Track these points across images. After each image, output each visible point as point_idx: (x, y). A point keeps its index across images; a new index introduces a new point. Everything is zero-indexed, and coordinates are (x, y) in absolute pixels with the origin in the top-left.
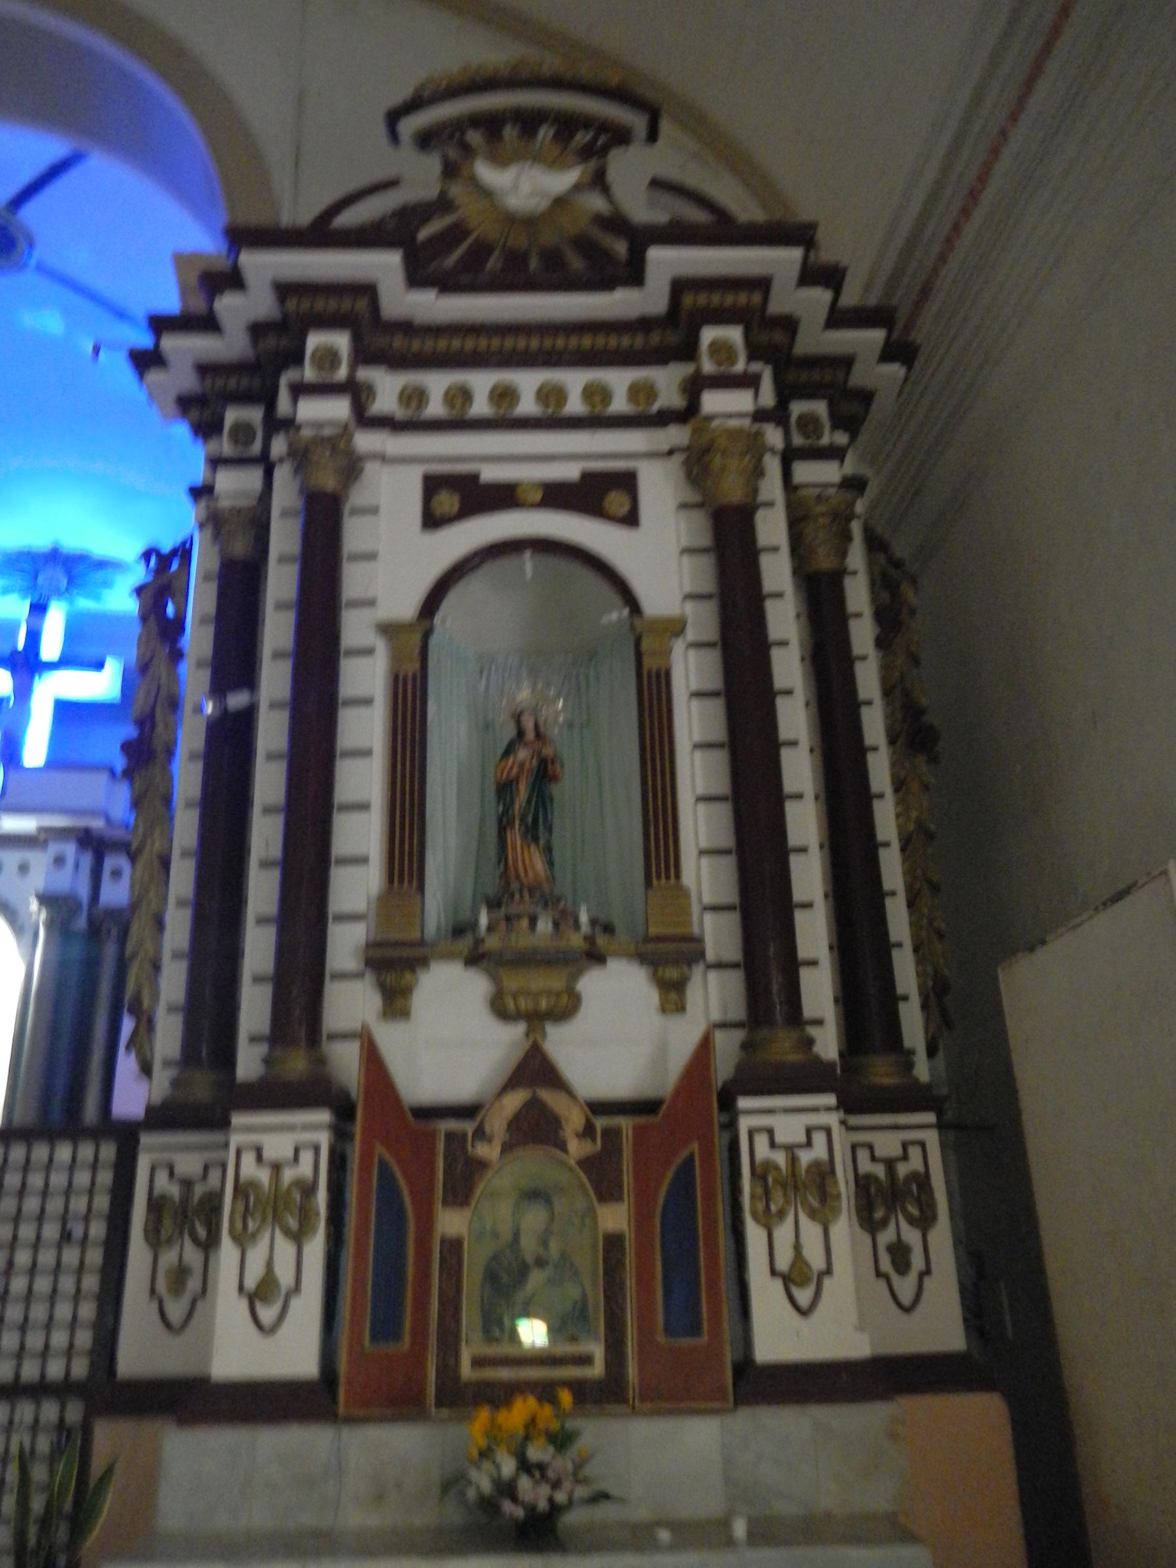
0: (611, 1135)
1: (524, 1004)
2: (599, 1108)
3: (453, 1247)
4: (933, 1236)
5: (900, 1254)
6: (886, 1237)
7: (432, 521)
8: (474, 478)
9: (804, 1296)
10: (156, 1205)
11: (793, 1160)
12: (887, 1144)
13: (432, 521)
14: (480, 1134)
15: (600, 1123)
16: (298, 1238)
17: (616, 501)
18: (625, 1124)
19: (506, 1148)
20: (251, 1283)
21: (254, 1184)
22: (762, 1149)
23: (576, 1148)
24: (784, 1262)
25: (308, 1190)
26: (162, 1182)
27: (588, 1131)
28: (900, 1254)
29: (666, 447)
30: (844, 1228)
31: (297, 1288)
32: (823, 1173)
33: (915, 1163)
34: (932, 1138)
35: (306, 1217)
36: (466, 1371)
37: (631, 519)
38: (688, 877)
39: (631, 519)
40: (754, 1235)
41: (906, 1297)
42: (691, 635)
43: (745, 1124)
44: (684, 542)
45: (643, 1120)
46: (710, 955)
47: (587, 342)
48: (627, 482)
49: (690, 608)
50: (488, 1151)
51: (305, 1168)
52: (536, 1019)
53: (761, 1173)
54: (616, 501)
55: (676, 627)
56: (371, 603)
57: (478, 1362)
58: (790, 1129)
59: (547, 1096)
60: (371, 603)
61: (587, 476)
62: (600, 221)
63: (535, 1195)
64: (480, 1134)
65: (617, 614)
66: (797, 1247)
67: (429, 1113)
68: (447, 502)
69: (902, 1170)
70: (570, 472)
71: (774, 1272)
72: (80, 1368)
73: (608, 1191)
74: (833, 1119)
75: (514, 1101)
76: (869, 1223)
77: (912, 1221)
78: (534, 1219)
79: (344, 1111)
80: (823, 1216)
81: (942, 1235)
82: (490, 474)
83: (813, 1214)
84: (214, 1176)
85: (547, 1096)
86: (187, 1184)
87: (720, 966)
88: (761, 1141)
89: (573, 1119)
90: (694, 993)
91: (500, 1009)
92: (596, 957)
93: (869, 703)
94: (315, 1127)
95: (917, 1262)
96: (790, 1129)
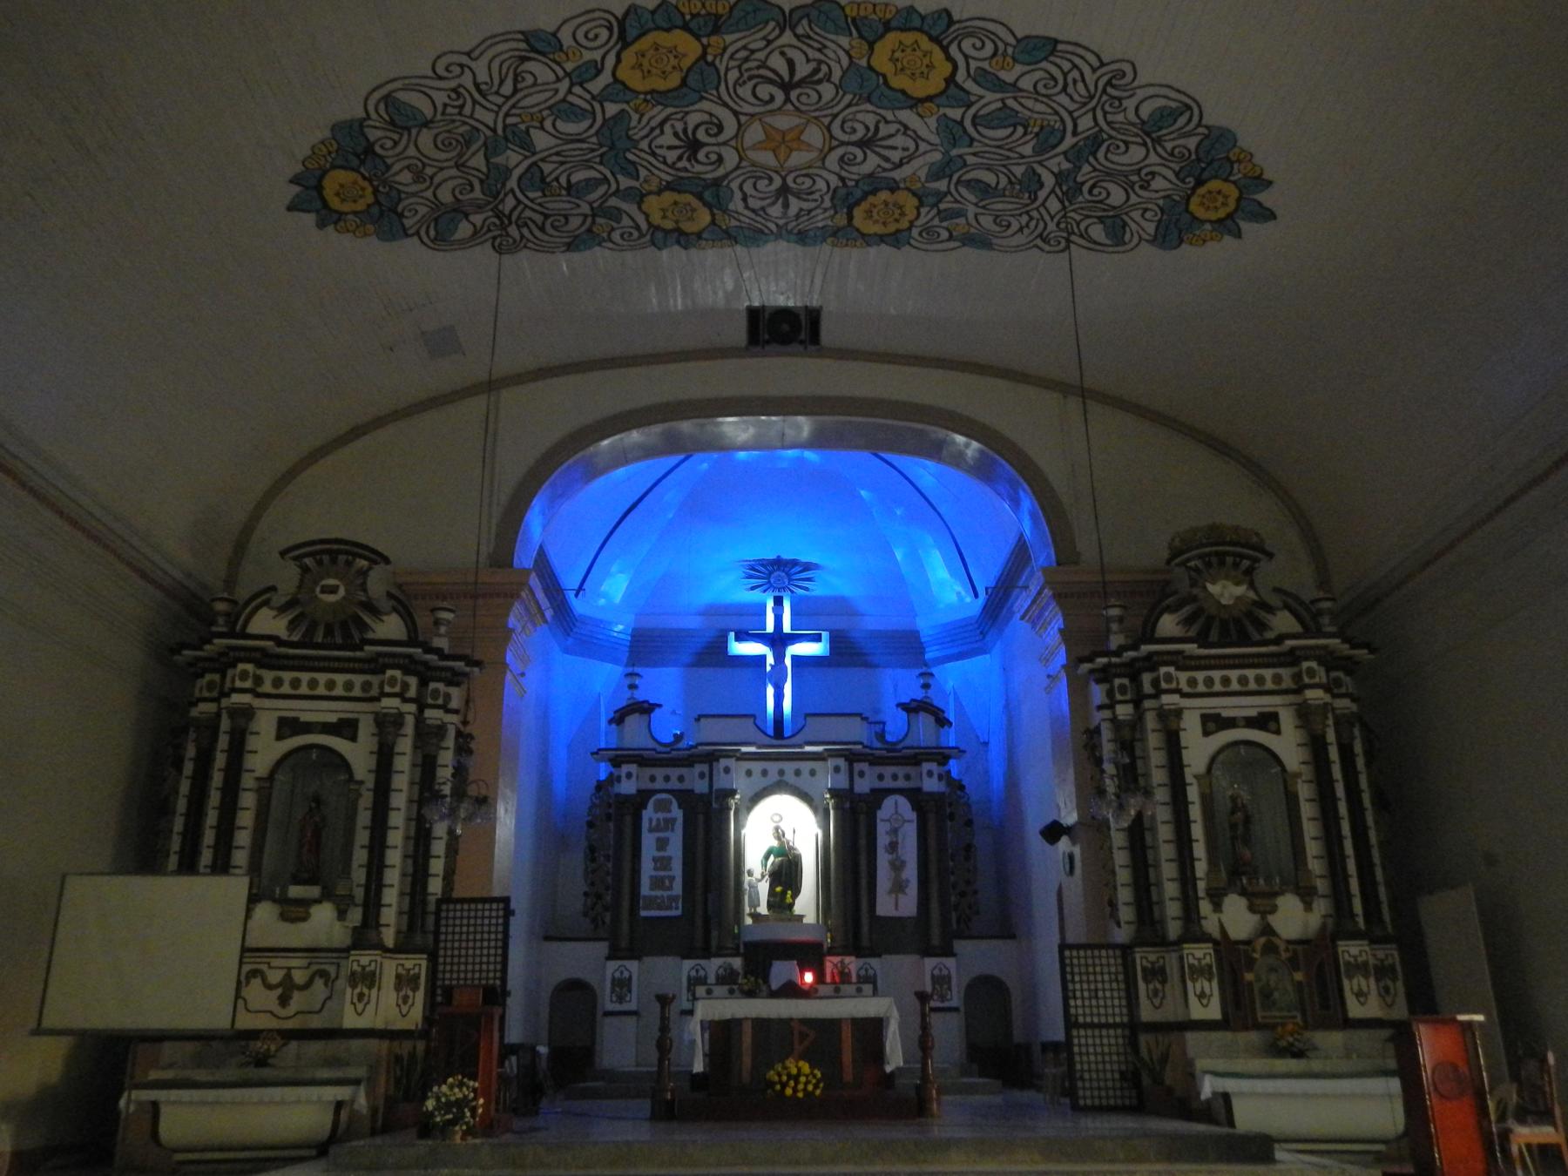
0: (1295, 952)
1: (1262, 909)
2: (1289, 942)
3: (1250, 984)
4: (417, 994)
5: (1387, 990)
6: (402, 993)
7: (1206, 733)
8: (1219, 715)
9: (1205, 1002)
10: (1144, 969)
11: (1356, 960)
12: (1381, 954)
13: (1206, 733)
14: (1254, 951)
15: (1291, 947)
16: (1210, 980)
17: (1272, 725)
18: (1300, 948)
19: (1262, 955)
20: (1198, 993)
21: (1193, 965)
22: (1191, 961)
23: (1284, 955)
24: (1356, 988)
25: (1210, 967)
26: (1145, 963)
27: (1287, 950)
28: (1387, 990)
29: (1288, 703)
30: (1372, 981)
31: (1211, 995)
32: (1366, 964)
33: (1390, 961)
34: (1396, 954)
35: (1211, 973)
36: (1260, 1020)
37: (1278, 732)
38: (1310, 866)
39: (1278, 732)
40: (1346, 983)
41: (359, 1010)
42: (1304, 778)
43: (1340, 949)
44: (1299, 741)
45: (1306, 946)
46: (1320, 892)
47: (322, 664)
48: (1274, 717)
49: (1303, 766)
50: (1256, 955)
51: (1208, 959)
52: (1264, 914)
53: (1191, 966)
54: (1272, 725)
55: (1298, 775)
56: (253, 771)
57: (1264, 1017)
58: (1354, 951)
59: (1273, 939)
60: (253, 771)
61: (341, 720)
62: (1255, 603)
63: (1272, 969)
64: (1254, 951)
65: (1278, 769)
66: (1359, 985)
67: (1238, 942)
68: (1211, 726)
69: (368, 969)
70: (1253, 713)
71: (1353, 992)
72: (1125, 1019)
73: (1296, 968)
74: (1367, 948)
75: (1262, 940)
76: (1378, 980)
77: (1160, 982)
78: (1273, 977)
79: (1216, 943)
80: (1366, 977)
81: (1400, 984)
82: (1225, 713)
83: (1363, 976)
84: (1161, 961)
85: (1273, 939)
86: (364, 968)
87: (1324, 896)
88: (1190, 957)
89: (1282, 946)
90: (1315, 905)
91: (1252, 909)
92: (1282, 893)
93: (1193, 803)
94: (1391, 949)
95: (1392, 991)
96: (1354, 951)
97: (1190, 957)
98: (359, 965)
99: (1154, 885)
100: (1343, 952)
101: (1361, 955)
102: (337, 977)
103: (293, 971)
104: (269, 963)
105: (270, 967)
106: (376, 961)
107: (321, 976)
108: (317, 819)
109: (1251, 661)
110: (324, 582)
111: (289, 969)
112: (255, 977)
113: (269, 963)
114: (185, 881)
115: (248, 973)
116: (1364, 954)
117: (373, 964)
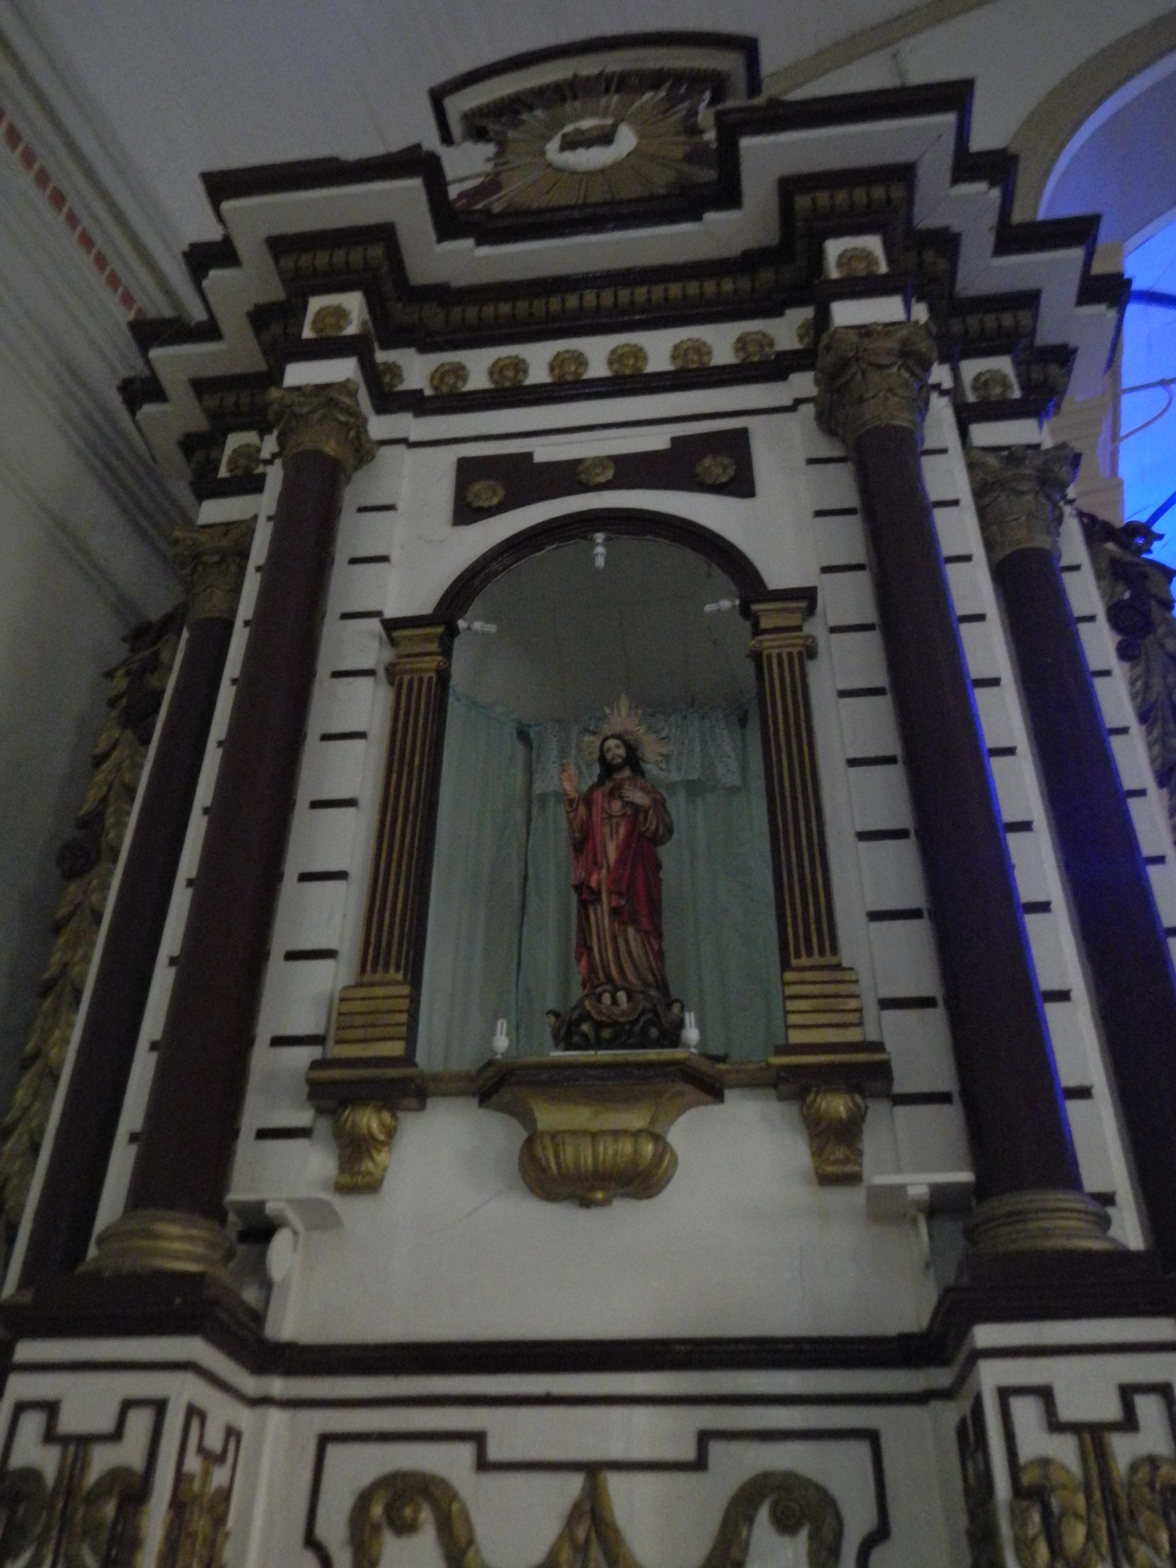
68: (484, 492)
82: (545, 451)
88: (1026, 1412)
97: (1026, 1412)
98: (50, 1436)
99: (596, 1053)
100: (1005, 1394)
101: (1129, 1422)
102: (880, 1534)
103: (616, 1485)
104: (478, 1438)
105: (483, 1465)
106: (160, 1406)
107: (785, 1524)
108: (638, 797)
109: (607, 298)
110: (569, 128)
111: (592, 1470)
112: (405, 1528)
113: (478, 1438)
114: (889, 1047)
115: (364, 1499)
116: (1149, 1408)
117: (139, 1423)
